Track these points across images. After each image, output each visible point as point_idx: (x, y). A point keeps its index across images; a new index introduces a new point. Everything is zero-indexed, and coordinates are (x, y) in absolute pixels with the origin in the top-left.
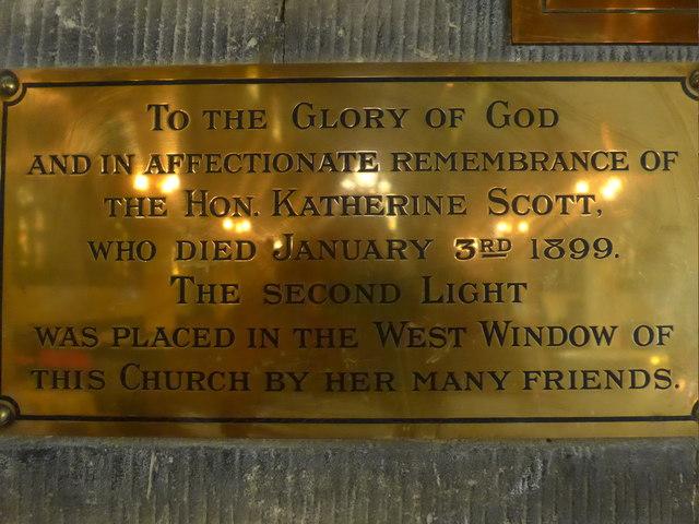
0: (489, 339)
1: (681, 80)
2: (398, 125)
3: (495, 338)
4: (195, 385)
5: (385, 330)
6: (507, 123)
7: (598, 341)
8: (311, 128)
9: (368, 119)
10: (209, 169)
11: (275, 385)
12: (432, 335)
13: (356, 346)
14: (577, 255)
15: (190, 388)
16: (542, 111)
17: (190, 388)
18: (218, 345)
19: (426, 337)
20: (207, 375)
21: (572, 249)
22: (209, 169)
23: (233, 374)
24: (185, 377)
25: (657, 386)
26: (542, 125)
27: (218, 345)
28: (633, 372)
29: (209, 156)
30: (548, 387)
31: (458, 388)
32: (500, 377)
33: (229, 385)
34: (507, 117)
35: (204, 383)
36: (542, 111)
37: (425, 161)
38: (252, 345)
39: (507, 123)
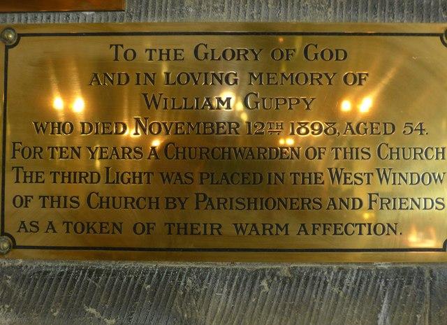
0: (381, 180)
1: (440, 35)
2: (256, 59)
3: (384, 180)
4: (129, 205)
5: (165, 177)
6: (316, 58)
7: (436, 181)
8: (205, 60)
9: (239, 55)
10: (269, 82)
11: (171, 205)
12: (355, 177)
13: (43, 182)
14: (316, 132)
15: (126, 207)
16: (337, 51)
17: (126, 207)
18: (254, 183)
19: (353, 179)
20: (136, 200)
21: (307, 129)
22: (269, 82)
23: (150, 198)
24: (123, 200)
25: (436, 208)
26: (337, 59)
27: (254, 183)
28: (425, 199)
29: (268, 74)
30: (382, 208)
31: (213, 208)
32: (183, 200)
33: (148, 206)
34: (316, 55)
35: (134, 204)
36: (337, 51)
37: (274, 78)
38: (17, 182)
39: (316, 58)
